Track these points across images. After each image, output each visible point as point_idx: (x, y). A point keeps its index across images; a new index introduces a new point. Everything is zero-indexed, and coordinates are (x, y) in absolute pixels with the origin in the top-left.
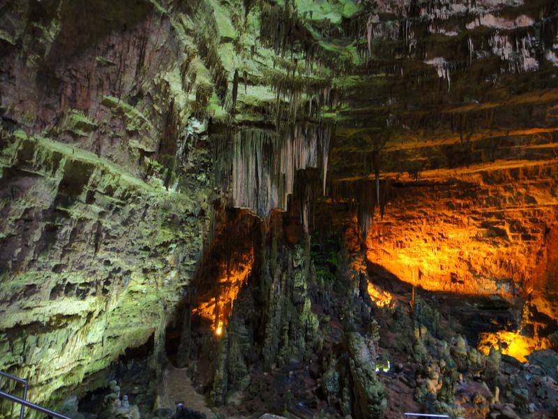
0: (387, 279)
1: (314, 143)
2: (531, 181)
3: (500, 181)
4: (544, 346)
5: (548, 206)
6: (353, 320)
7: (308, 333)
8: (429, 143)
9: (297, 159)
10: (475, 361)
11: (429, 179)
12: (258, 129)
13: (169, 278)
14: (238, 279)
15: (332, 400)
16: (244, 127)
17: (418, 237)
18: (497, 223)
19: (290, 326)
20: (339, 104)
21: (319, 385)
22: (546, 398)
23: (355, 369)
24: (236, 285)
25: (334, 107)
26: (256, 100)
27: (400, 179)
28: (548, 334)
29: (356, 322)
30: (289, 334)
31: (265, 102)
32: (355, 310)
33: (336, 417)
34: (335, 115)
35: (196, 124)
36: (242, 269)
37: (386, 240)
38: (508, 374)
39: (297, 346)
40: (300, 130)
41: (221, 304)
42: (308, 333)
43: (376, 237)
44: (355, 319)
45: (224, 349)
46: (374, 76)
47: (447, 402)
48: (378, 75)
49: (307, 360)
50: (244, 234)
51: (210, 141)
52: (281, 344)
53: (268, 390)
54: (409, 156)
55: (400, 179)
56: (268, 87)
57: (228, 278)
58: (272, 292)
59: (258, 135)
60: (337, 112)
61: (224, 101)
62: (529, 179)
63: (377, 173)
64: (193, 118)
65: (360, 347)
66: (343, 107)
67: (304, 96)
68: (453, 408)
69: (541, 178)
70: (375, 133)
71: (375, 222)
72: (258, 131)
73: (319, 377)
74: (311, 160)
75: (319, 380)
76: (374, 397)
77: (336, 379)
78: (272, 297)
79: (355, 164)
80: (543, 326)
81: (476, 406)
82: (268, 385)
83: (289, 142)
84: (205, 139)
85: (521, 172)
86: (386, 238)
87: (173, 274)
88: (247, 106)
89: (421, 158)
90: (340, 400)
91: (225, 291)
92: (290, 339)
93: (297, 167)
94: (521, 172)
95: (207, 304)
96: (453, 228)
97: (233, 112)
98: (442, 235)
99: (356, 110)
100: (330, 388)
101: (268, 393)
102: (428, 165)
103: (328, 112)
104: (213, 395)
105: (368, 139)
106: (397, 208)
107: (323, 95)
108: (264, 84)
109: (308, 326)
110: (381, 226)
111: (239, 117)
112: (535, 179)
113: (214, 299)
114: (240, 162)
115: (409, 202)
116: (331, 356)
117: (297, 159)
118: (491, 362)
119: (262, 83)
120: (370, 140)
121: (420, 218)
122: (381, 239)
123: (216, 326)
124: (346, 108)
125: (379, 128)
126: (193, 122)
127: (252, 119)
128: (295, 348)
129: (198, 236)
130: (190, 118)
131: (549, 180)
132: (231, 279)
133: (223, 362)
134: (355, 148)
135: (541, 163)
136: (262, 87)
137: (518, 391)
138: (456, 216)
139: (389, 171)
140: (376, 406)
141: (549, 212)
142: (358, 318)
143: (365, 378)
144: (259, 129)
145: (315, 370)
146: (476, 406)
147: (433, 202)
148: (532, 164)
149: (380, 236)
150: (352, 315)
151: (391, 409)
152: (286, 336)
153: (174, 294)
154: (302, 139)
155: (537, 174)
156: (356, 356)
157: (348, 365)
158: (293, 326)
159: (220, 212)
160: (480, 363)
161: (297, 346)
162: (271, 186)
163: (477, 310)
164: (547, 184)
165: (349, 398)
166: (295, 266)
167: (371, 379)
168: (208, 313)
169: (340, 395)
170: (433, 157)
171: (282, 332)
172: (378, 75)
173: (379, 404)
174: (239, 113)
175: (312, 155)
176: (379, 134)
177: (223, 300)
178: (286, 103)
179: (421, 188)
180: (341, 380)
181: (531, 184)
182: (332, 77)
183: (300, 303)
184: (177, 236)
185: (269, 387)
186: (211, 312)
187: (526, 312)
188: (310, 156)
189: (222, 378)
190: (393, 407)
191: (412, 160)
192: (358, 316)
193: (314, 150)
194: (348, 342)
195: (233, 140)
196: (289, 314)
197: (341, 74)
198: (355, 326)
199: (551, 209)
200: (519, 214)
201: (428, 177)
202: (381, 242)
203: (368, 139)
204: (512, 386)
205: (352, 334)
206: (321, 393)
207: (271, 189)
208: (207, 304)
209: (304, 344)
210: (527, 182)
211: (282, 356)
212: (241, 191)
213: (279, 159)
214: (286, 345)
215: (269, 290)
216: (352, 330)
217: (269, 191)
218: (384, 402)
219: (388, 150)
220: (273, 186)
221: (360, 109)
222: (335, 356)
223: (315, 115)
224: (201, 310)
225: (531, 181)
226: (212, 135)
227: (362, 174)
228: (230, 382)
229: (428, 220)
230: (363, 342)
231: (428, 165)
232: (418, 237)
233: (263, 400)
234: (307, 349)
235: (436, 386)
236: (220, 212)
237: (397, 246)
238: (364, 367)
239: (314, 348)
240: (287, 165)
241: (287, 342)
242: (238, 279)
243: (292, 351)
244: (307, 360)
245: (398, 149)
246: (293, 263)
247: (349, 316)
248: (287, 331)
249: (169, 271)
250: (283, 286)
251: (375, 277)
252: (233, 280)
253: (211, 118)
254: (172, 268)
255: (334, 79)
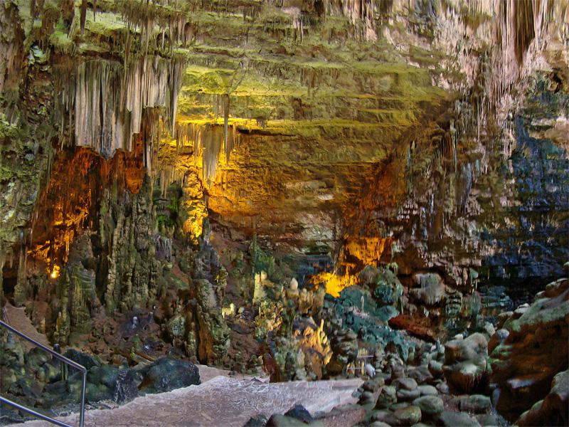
0: (227, 227)
1: (164, 78)
2: (359, 141)
3: (335, 138)
4: (352, 283)
5: (369, 163)
6: (202, 268)
7: (152, 280)
8: (278, 93)
9: (144, 96)
10: (305, 300)
11: (274, 128)
12: (104, 60)
13: (7, 217)
14: (73, 223)
15: (177, 343)
16: (88, 57)
17: (259, 186)
18: (328, 176)
19: (133, 272)
20: (193, 39)
21: (163, 329)
22: (353, 323)
23: (201, 314)
24: (72, 229)
25: (187, 43)
26: (103, 29)
27: (247, 126)
28: (356, 272)
29: (205, 269)
30: (132, 281)
31: (112, 31)
32: (204, 257)
33: (182, 358)
34: (188, 51)
35: (39, 53)
36: (78, 212)
37: (228, 187)
38: (327, 309)
39: (140, 292)
40: (150, 63)
41: (56, 247)
42: (152, 280)
43: (219, 185)
44: (203, 266)
45: (66, 293)
46: (231, 15)
47: (286, 336)
48: (235, 15)
49: (151, 306)
50: (81, 174)
51: (51, 72)
52: (124, 290)
53: (111, 334)
54: (258, 103)
55: (247, 126)
56: (119, 15)
57: (64, 221)
58: (115, 238)
59: (104, 67)
60: (191, 48)
61: (69, 29)
62: (357, 138)
63: (226, 117)
64: (36, 47)
65: (208, 294)
66: (197, 44)
67: (157, 29)
68: (290, 341)
69: (366, 138)
70: (228, 74)
71: (220, 169)
72: (105, 62)
73: (163, 322)
74: (160, 98)
75: (163, 325)
76: (220, 338)
77: (182, 323)
78: (115, 243)
79: (204, 106)
80: (353, 266)
81: (306, 337)
82: (112, 329)
83: (137, 76)
84: (46, 69)
85: (351, 131)
86: (229, 185)
87: (11, 214)
88: (94, 35)
89: (269, 107)
90: (185, 343)
91: (60, 235)
92: (133, 285)
93: (145, 104)
94: (351, 131)
95: (41, 246)
96: (291, 178)
97: (77, 40)
98: (281, 185)
99: (211, 48)
100: (176, 332)
101: (112, 337)
102: (275, 114)
103: (181, 46)
104: (57, 336)
105: (219, 80)
106: (242, 155)
107: (177, 29)
108: (114, 10)
109: (152, 273)
110: (225, 172)
111: (83, 47)
112: (361, 139)
113: (49, 242)
114: (84, 96)
115: (254, 150)
116: (177, 302)
117: (144, 96)
118: (318, 299)
119: (112, 10)
120: (222, 82)
121: (262, 167)
122: (224, 186)
123: (52, 271)
124: (200, 45)
125: (232, 71)
126: (35, 51)
127: (97, 49)
128: (138, 295)
129: (35, 175)
130: (32, 46)
131: (371, 141)
132: (67, 222)
133: (66, 305)
134: (206, 89)
135: (368, 125)
136: (111, 15)
137: (335, 321)
138: (295, 167)
139: (238, 116)
140: (221, 346)
141: (369, 168)
142: (207, 266)
143: (212, 322)
144: (105, 61)
145: (160, 316)
146: (306, 337)
147: (275, 151)
148: (359, 125)
149: (223, 183)
150: (201, 262)
151: (234, 348)
152: (130, 283)
153: (11, 234)
154: (151, 74)
155: (363, 135)
156: (203, 302)
157: (194, 310)
158: (137, 273)
159: (58, 150)
160: (309, 301)
161: (140, 292)
162: (116, 123)
163: (305, 256)
164: (370, 144)
165: (195, 341)
166: (140, 211)
167: (218, 322)
168: (43, 256)
169: (186, 337)
170: (280, 107)
171: (125, 279)
172: (235, 15)
173: (224, 344)
174: (83, 42)
175: (161, 92)
176: (231, 77)
177: (58, 243)
178: (137, 34)
179: (266, 137)
180: (187, 325)
181: (358, 143)
182: (187, 10)
183: (144, 250)
184: (15, 175)
185: (113, 332)
186: (46, 255)
187: (342, 254)
188: (159, 96)
189: (65, 320)
190: (236, 346)
191: (261, 107)
192: (207, 264)
193: (163, 87)
194: (196, 289)
195: (76, 72)
196: (133, 261)
197: (198, 8)
198: (204, 273)
199: (370, 166)
200: (346, 169)
201: (274, 126)
202: (224, 189)
203: (219, 80)
204: (331, 317)
205: (201, 281)
206: (166, 336)
207: (116, 128)
208: (41, 246)
209: (147, 291)
210: (355, 140)
211: (125, 302)
212: (84, 128)
213: (126, 94)
214: (130, 292)
215: (112, 236)
216: (201, 276)
217: (114, 129)
218: (228, 342)
219: (238, 95)
220: (118, 124)
221: (214, 48)
222: (181, 302)
223: (167, 49)
224: (35, 253)
225: (359, 141)
226: (54, 65)
227: (210, 117)
228: (72, 324)
229: (270, 170)
230: (211, 289)
231: (275, 114)
232: (259, 186)
233: (107, 343)
234: (150, 296)
235: (273, 325)
236: (58, 150)
237: (240, 194)
238: (212, 312)
239: (157, 295)
240: (134, 102)
241: (130, 288)
242: (73, 223)
243: (135, 297)
244: (151, 306)
245: (248, 94)
246: (138, 209)
247: (199, 264)
248: (130, 278)
249: (7, 211)
250: (127, 232)
251: (215, 225)
252: (69, 223)
253: (53, 46)
254: (10, 208)
255: (189, 13)
